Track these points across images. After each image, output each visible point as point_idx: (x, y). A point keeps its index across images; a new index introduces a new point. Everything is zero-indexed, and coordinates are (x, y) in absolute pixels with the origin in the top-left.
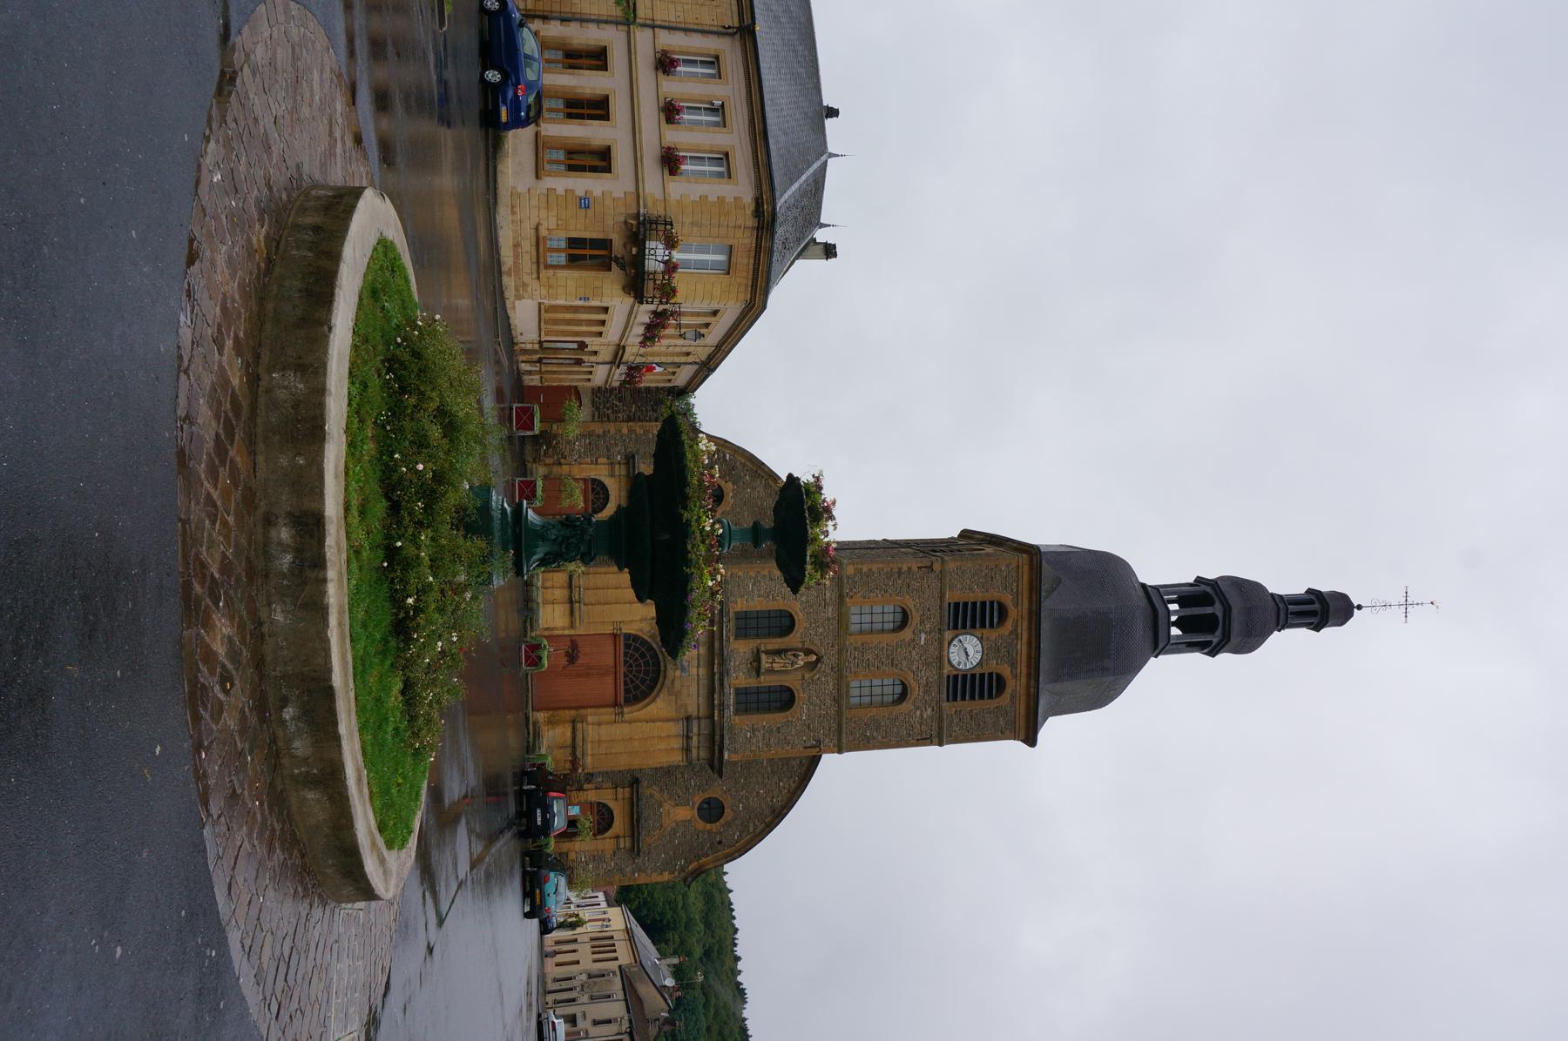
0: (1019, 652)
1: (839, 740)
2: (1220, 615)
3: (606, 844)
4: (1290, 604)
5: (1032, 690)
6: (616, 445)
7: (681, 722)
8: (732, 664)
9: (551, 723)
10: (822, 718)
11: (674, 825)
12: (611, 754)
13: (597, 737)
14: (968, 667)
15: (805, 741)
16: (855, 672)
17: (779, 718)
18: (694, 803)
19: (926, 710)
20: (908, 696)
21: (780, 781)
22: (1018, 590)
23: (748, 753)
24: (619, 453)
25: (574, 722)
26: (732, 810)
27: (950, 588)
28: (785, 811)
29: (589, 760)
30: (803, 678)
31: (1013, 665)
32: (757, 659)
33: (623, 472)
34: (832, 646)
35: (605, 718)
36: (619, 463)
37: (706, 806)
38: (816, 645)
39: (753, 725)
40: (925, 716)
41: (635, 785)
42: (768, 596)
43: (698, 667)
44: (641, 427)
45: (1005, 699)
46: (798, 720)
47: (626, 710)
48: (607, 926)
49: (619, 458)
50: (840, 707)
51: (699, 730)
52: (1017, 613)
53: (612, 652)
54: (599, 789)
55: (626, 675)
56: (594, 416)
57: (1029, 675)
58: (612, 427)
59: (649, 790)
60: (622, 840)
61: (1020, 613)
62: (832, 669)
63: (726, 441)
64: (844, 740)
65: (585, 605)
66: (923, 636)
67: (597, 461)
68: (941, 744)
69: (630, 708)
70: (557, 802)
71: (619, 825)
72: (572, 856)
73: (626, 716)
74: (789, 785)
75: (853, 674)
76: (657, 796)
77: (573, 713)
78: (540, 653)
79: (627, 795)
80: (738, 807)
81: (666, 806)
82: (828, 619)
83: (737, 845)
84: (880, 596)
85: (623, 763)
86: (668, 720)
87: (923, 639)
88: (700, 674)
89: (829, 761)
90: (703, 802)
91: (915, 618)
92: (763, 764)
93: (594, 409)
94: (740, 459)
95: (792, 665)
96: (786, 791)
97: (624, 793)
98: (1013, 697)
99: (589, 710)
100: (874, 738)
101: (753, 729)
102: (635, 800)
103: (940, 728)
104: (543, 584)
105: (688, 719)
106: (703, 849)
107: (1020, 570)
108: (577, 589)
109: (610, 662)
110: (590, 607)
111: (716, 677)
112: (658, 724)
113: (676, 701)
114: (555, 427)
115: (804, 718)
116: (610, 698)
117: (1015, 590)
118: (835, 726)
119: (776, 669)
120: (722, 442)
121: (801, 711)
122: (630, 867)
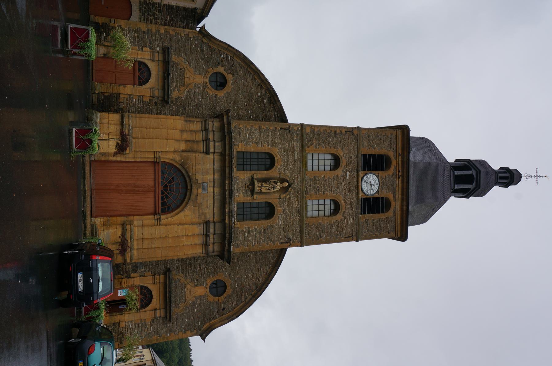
0: (397, 185)
1: (302, 238)
2: (474, 174)
3: (147, 314)
4: (499, 173)
5: (404, 208)
6: (156, 40)
7: (202, 225)
8: (236, 186)
9: (106, 225)
10: (291, 224)
11: (194, 299)
12: (152, 248)
13: (141, 236)
14: (372, 194)
15: (281, 239)
16: (311, 195)
17: (266, 223)
18: (207, 284)
19: (350, 219)
20: (340, 210)
21: (261, 267)
22: (396, 148)
23: (245, 247)
24: (158, 46)
25: (123, 225)
26: (232, 287)
27: (362, 146)
28: (264, 286)
29: (135, 253)
30: (280, 198)
31: (394, 193)
32: (252, 183)
33: (161, 58)
34: (297, 178)
35: (146, 222)
36: (158, 52)
37: (214, 286)
38: (288, 176)
39: (249, 228)
40: (349, 223)
41: (167, 273)
42: (258, 143)
43: (214, 187)
44: (173, 30)
45: (390, 214)
46: (276, 225)
47: (162, 217)
48: (142, 359)
49: (158, 49)
50: (301, 216)
51: (214, 231)
52: (396, 163)
53: (153, 176)
54: (143, 276)
55: (162, 193)
56: (140, 19)
57: (402, 199)
58: (153, 28)
59: (177, 277)
60: (158, 311)
61: (398, 163)
62: (297, 192)
63: (229, 46)
64: (304, 238)
65: (133, 138)
66: (348, 173)
67: (142, 49)
68: (357, 240)
69: (165, 216)
70: (102, 265)
71: (156, 302)
72: (123, 325)
73: (163, 221)
74: (266, 270)
75: (309, 196)
76: (183, 280)
77: (123, 218)
78: (90, 136)
79: (162, 280)
80: (235, 285)
81: (189, 287)
82: (295, 160)
83: (234, 310)
84: (324, 147)
85: (161, 254)
86: (193, 224)
87: (348, 175)
88: (215, 192)
89: (291, 252)
90: (213, 283)
91: (344, 162)
92: (250, 257)
93: (141, 14)
94: (237, 60)
95: (274, 188)
96: (264, 274)
97: (160, 278)
98: (394, 212)
99: (135, 217)
100: (321, 236)
101: (249, 231)
102: (167, 283)
103: (357, 230)
104: (101, 121)
105: (207, 223)
106: (213, 314)
107: (398, 137)
108: (127, 126)
109: (152, 183)
110: (137, 140)
111: (227, 193)
112: (186, 226)
113: (198, 210)
114: (112, 21)
115: (280, 224)
116: (152, 210)
117: (395, 149)
118: (299, 229)
119: (263, 191)
120: (226, 47)
121: (279, 218)
122: (164, 329)
